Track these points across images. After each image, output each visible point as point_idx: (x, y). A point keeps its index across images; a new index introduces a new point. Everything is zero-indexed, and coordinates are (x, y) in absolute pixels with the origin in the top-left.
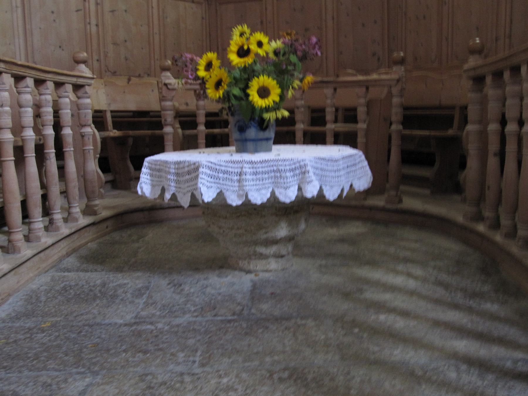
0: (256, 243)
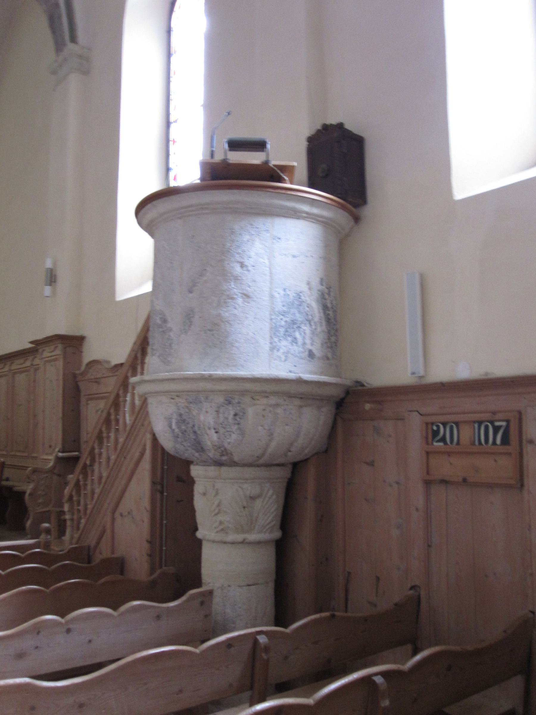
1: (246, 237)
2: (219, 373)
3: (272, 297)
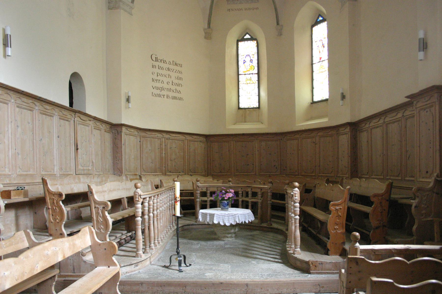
0: (226, 233)
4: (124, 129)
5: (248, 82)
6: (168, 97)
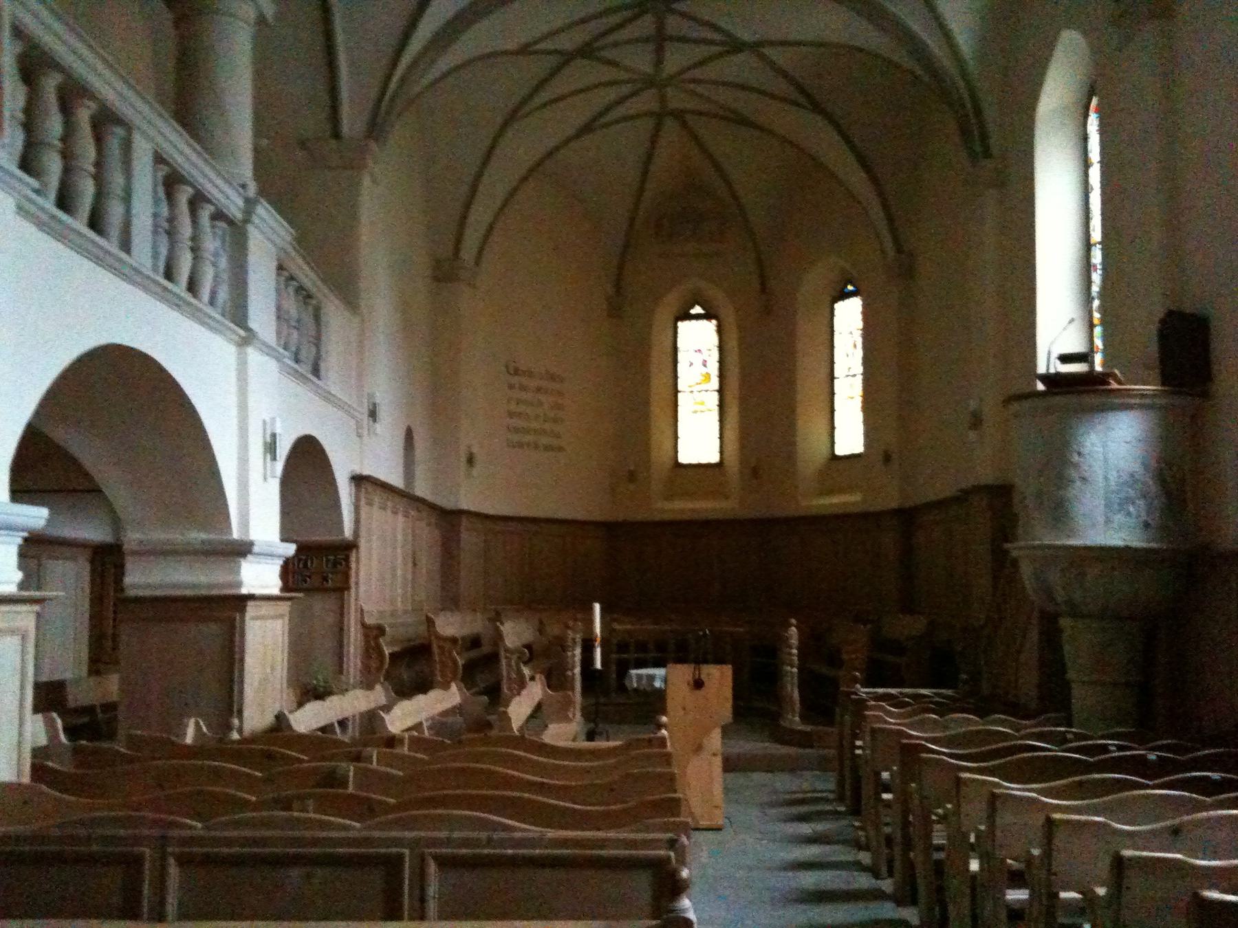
1: (1081, 431)
2: (1058, 543)
3: (1106, 478)
4: (465, 521)
5: (699, 408)
6: (536, 447)
